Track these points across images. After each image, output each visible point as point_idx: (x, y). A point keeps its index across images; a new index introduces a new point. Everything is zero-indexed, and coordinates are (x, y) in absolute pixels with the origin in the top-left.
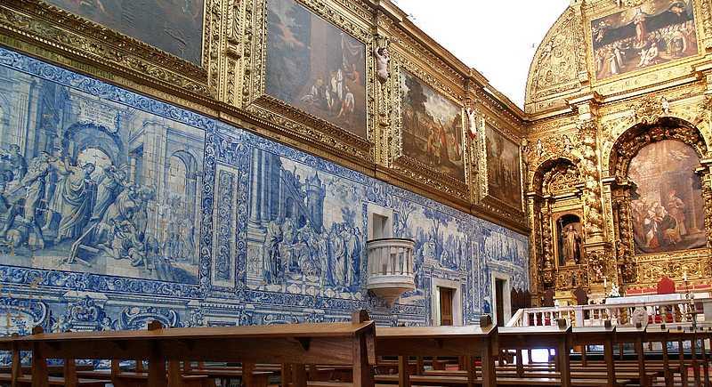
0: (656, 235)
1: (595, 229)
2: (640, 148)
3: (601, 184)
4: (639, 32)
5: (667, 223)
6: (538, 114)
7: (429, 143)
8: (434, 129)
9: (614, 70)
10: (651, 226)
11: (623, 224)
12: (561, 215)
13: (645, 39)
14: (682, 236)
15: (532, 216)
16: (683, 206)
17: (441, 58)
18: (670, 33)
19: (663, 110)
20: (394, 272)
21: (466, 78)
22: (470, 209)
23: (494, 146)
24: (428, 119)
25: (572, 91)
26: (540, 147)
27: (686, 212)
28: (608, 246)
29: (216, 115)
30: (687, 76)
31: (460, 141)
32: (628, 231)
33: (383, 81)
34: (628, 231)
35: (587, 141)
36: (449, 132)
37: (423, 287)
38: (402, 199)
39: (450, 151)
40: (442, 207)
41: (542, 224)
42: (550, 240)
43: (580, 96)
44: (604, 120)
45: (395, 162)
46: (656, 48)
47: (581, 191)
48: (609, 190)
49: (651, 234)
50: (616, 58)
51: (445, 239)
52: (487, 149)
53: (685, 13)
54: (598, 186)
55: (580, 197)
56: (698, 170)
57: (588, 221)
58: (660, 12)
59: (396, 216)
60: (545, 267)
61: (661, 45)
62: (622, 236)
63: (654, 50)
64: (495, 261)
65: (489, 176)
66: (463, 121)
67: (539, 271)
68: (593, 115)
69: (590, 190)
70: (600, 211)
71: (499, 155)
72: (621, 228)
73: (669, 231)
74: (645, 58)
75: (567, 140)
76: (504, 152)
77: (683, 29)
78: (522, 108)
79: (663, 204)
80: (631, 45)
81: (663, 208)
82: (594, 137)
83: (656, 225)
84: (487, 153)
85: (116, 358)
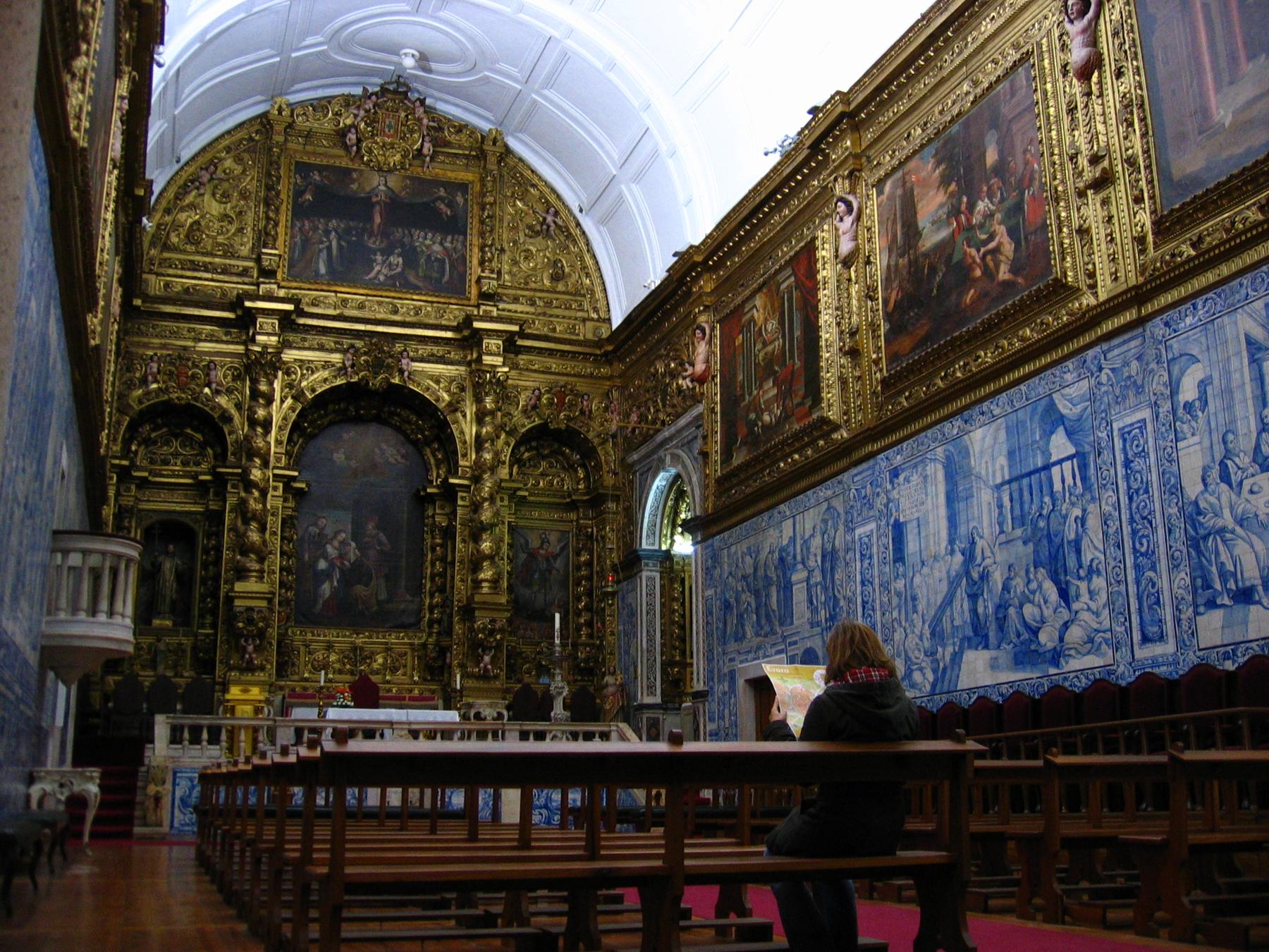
0: (335, 592)
2: (331, 424)
4: (378, 220)
5: (353, 575)
9: (323, 270)
10: (327, 575)
12: (155, 517)
13: (385, 234)
14: (379, 603)
18: (428, 242)
20: (93, 611)
25: (235, 279)
26: (155, 370)
46: (400, 260)
49: (326, 588)
50: (329, 248)
53: (454, 217)
58: (418, 200)
63: (397, 260)
73: (360, 589)
74: (379, 270)
77: (448, 245)
79: (356, 536)
81: (353, 544)
83: (337, 575)
85: (405, 785)
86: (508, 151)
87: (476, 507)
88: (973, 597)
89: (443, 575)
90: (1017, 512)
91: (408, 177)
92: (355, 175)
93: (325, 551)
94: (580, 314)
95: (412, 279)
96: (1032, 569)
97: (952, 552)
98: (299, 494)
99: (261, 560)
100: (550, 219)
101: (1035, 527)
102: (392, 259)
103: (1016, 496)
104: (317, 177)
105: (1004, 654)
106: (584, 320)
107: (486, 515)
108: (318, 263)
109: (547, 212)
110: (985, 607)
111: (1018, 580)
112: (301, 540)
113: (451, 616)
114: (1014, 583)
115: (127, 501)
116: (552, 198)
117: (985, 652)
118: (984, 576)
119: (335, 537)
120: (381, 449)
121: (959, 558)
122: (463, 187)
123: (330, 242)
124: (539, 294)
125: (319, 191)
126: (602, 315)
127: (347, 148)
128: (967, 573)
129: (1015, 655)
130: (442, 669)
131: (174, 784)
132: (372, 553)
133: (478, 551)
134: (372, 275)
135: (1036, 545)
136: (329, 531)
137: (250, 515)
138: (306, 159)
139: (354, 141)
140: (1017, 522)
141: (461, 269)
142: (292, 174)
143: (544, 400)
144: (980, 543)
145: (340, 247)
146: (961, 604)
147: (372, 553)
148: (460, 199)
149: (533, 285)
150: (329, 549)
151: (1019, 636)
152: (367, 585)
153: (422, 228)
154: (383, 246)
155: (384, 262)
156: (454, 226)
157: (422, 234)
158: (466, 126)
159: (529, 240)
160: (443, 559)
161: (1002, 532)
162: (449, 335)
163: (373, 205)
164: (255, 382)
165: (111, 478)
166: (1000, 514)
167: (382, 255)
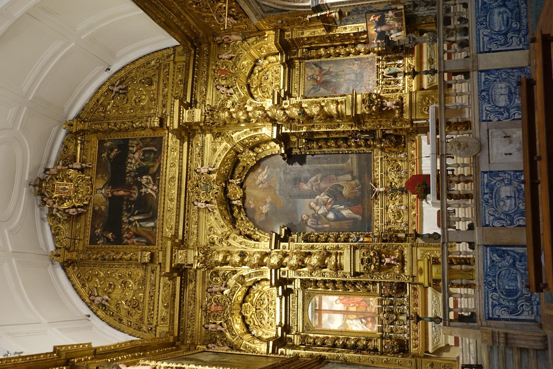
0: (348, 207)
1: (331, 261)
4: (122, 193)
9: (152, 224)
10: (337, 213)
14: (353, 178)
18: (133, 161)
26: (214, 326)
46: (144, 177)
49: (346, 213)
50: (139, 221)
53: (119, 147)
58: (110, 170)
61: (142, 171)
63: (144, 179)
73: (345, 192)
74: (150, 190)
77: (135, 149)
79: (312, 196)
80: (131, 203)
81: (318, 197)
83: (337, 207)
86: (78, 117)
87: (290, 120)
89: (336, 140)
91: (97, 178)
92: (97, 208)
93: (322, 214)
94: (172, 66)
95: (155, 169)
98: (288, 232)
99: (329, 254)
100: (115, 89)
102: (144, 183)
104: (99, 230)
106: (175, 63)
107: (295, 112)
112: (317, 230)
113: (362, 132)
115: (297, 340)
116: (105, 88)
119: (313, 209)
120: (259, 185)
122: (101, 142)
123: (135, 220)
125: (106, 229)
126: (171, 52)
127: (79, 215)
130: (398, 137)
132: (323, 185)
133: (318, 115)
134: (154, 194)
136: (311, 212)
137: (300, 263)
138: (88, 239)
139: (74, 210)
141: (148, 140)
142: (96, 246)
145: (138, 214)
148: (108, 144)
150: (320, 212)
154: (136, 188)
155: (146, 187)
156: (124, 147)
157: (129, 165)
158: (63, 143)
160: (326, 140)
162: (186, 144)
163: (113, 196)
164: (217, 263)
165: (282, 353)
167: (142, 188)
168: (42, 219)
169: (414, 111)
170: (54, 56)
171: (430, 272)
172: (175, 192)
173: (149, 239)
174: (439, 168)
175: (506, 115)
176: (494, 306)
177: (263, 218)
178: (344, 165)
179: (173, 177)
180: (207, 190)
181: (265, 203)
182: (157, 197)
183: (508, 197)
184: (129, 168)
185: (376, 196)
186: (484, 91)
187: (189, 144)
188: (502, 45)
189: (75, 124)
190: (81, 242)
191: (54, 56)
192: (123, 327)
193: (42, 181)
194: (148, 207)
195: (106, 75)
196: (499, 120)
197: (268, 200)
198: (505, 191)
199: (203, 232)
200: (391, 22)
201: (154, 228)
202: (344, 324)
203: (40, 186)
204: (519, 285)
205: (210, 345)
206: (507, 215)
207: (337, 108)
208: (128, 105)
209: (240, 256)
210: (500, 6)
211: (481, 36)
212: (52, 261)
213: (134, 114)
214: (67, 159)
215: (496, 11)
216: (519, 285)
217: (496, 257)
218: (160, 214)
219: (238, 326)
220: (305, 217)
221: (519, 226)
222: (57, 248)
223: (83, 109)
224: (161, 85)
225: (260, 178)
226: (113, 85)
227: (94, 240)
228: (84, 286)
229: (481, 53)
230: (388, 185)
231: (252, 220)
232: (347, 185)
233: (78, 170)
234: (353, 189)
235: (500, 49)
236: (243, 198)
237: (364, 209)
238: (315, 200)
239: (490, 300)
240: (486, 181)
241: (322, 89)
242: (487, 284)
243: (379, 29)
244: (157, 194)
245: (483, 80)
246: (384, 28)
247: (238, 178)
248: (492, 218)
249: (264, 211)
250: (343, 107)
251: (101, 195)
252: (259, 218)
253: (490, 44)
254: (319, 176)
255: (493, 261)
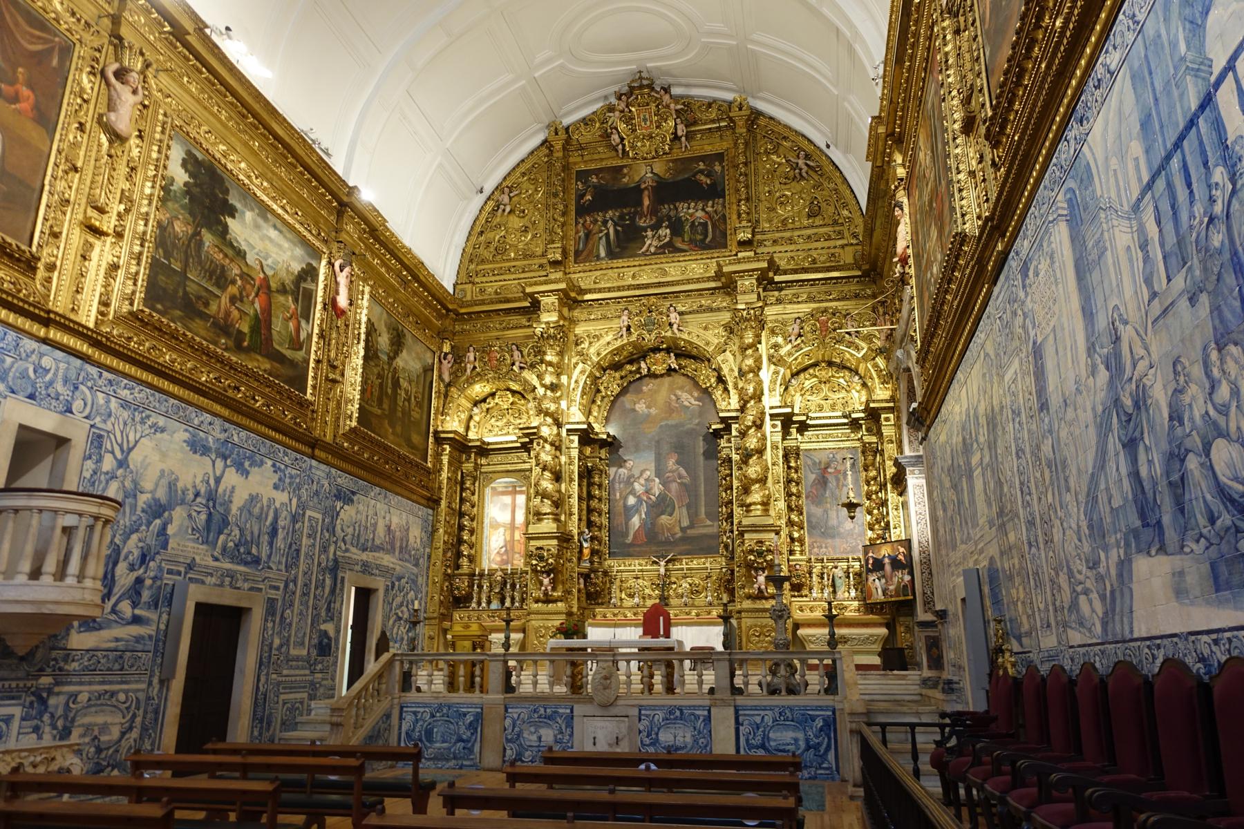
0: (643, 524)
3: (564, 433)
4: (646, 202)
5: (661, 505)
6: (475, 303)
7: (225, 300)
8: (246, 277)
9: (603, 253)
10: (636, 508)
11: (594, 503)
14: (683, 530)
15: (445, 475)
16: (687, 480)
17: (287, 146)
18: (691, 211)
19: (671, 325)
20: (61, 574)
21: (342, 204)
22: (312, 445)
23: (384, 341)
24: (230, 252)
26: (472, 358)
27: (689, 490)
28: (564, 538)
29: (42, 333)
30: (709, 279)
31: (307, 315)
32: (600, 515)
33: (117, 138)
34: (600, 515)
35: (548, 358)
36: (283, 290)
37: (155, 604)
38: (125, 404)
39: (277, 325)
40: (238, 436)
41: (462, 490)
42: (472, 520)
43: (546, 283)
44: (579, 330)
45: (119, 319)
46: (668, 231)
47: (531, 442)
48: (576, 444)
49: (636, 521)
50: (607, 235)
51: (238, 501)
52: (367, 341)
53: (713, 186)
54: (559, 434)
55: (528, 451)
56: (714, 427)
57: (537, 493)
58: (680, 178)
59: (97, 440)
60: (458, 567)
62: (590, 524)
63: (665, 232)
64: (356, 554)
65: (363, 392)
66: (321, 278)
67: (446, 574)
68: (562, 317)
69: (546, 441)
70: (557, 477)
71: (391, 359)
72: (590, 511)
73: (664, 519)
74: (651, 243)
75: (516, 353)
76: (404, 354)
77: (709, 209)
78: (448, 285)
79: (659, 474)
80: (632, 219)
81: (657, 480)
82: (561, 354)
83: (644, 508)
84: (367, 349)
88: (1131, 445)
90: (1171, 239)
91: (668, 161)
92: (625, 171)
95: (679, 245)
96: (1214, 355)
97: (1093, 372)
100: (801, 162)
101: (1206, 251)
103: (1165, 207)
105: (1194, 568)
106: (843, 247)
108: (598, 250)
109: (798, 157)
110: (1150, 462)
111: (1193, 389)
114: (1186, 399)
117: (1163, 559)
118: (1141, 401)
121: (1103, 375)
122: (720, 157)
124: (797, 233)
128: (1117, 402)
129: (1213, 566)
131: (401, 718)
132: (674, 486)
135: (1214, 294)
138: (583, 167)
139: (618, 140)
140: (1173, 261)
143: (807, 328)
144: (1127, 333)
145: (616, 231)
146: (1119, 465)
147: (674, 486)
148: (718, 168)
149: (790, 226)
150: (636, 486)
151: (1212, 520)
152: (671, 515)
153: (684, 200)
158: (715, 101)
159: (783, 187)
161: (1154, 295)
162: (713, 285)
163: (643, 190)
166: (1146, 259)
168: (606, 97)
169: (754, 615)
170: (812, 67)
171: (465, 638)
172: (644, 280)
173: (583, 254)
174: (621, 650)
175: (647, 741)
176: (415, 713)
177: (628, 406)
178: (703, 516)
179: (665, 273)
180: (646, 325)
181: (649, 407)
182: (640, 255)
183: (540, 738)
184: (682, 206)
185: (654, 562)
186: (682, 713)
187: (714, 289)
188: (747, 740)
189: (743, 113)
190: (579, 159)
191: (812, 67)
192: (473, 239)
193: (651, 87)
194: (626, 244)
195: (821, 142)
196: (640, 732)
197: (653, 411)
198: (548, 735)
199: (591, 328)
200: (895, 580)
201: (598, 258)
202: (495, 525)
203: (641, 87)
204: (438, 745)
205: (450, 356)
206: (518, 735)
207: (754, 504)
208: (777, 186)
209: (552, 384)
210: (807, 741)
211: (762, 713)
212: (548, 126)
213: (763, 198)
214: (688, 111)
215: (800, 735)
216: (438, 745)
217: (469, 718)
218: (616, 263)
219: (479, 389)
220: (629, 464)
221: (505, 749)
222: (567, 129)
223: (771, 118)
224: (809, 232)
225: (684, 396)
226: (807, 157)
227: (583, 175)
228: (524, 174)
229: (737, 711)
230: (673, 579)
231: (624, 391)
232: (674, 521)
233: (675, 133)
234: (669, 530)
235: (742, 739)
236: (652, 375)
237: (639, 546)
238: (653, 476)
239: (422, 710)
240: (561, 711)
241: (814, 476)
242: (440, 706)
243: (887, 560)
244: (644, 254)
245: (697, 712)
246: (888, 568)
247: (679, 365)
248: (516, 716)
249: (638, 407)
250: (759, 513)
251: (643, 173)
252: (627, 400)
253: (750, 724)
254: (687, 480)
255: (465, 715)
